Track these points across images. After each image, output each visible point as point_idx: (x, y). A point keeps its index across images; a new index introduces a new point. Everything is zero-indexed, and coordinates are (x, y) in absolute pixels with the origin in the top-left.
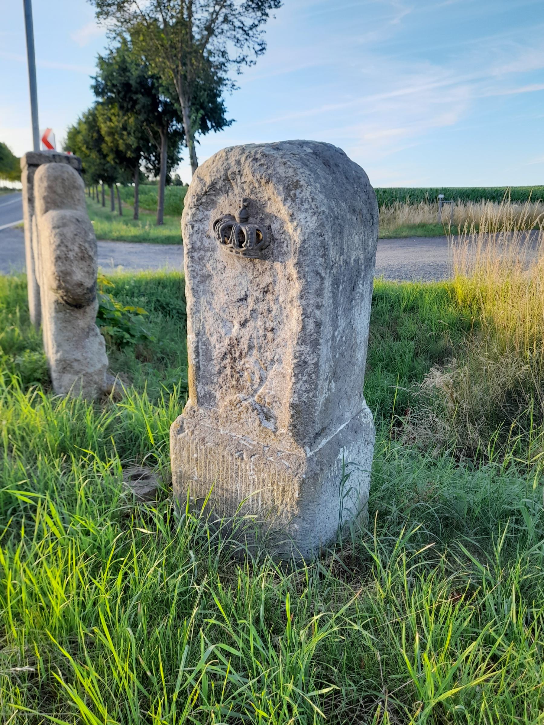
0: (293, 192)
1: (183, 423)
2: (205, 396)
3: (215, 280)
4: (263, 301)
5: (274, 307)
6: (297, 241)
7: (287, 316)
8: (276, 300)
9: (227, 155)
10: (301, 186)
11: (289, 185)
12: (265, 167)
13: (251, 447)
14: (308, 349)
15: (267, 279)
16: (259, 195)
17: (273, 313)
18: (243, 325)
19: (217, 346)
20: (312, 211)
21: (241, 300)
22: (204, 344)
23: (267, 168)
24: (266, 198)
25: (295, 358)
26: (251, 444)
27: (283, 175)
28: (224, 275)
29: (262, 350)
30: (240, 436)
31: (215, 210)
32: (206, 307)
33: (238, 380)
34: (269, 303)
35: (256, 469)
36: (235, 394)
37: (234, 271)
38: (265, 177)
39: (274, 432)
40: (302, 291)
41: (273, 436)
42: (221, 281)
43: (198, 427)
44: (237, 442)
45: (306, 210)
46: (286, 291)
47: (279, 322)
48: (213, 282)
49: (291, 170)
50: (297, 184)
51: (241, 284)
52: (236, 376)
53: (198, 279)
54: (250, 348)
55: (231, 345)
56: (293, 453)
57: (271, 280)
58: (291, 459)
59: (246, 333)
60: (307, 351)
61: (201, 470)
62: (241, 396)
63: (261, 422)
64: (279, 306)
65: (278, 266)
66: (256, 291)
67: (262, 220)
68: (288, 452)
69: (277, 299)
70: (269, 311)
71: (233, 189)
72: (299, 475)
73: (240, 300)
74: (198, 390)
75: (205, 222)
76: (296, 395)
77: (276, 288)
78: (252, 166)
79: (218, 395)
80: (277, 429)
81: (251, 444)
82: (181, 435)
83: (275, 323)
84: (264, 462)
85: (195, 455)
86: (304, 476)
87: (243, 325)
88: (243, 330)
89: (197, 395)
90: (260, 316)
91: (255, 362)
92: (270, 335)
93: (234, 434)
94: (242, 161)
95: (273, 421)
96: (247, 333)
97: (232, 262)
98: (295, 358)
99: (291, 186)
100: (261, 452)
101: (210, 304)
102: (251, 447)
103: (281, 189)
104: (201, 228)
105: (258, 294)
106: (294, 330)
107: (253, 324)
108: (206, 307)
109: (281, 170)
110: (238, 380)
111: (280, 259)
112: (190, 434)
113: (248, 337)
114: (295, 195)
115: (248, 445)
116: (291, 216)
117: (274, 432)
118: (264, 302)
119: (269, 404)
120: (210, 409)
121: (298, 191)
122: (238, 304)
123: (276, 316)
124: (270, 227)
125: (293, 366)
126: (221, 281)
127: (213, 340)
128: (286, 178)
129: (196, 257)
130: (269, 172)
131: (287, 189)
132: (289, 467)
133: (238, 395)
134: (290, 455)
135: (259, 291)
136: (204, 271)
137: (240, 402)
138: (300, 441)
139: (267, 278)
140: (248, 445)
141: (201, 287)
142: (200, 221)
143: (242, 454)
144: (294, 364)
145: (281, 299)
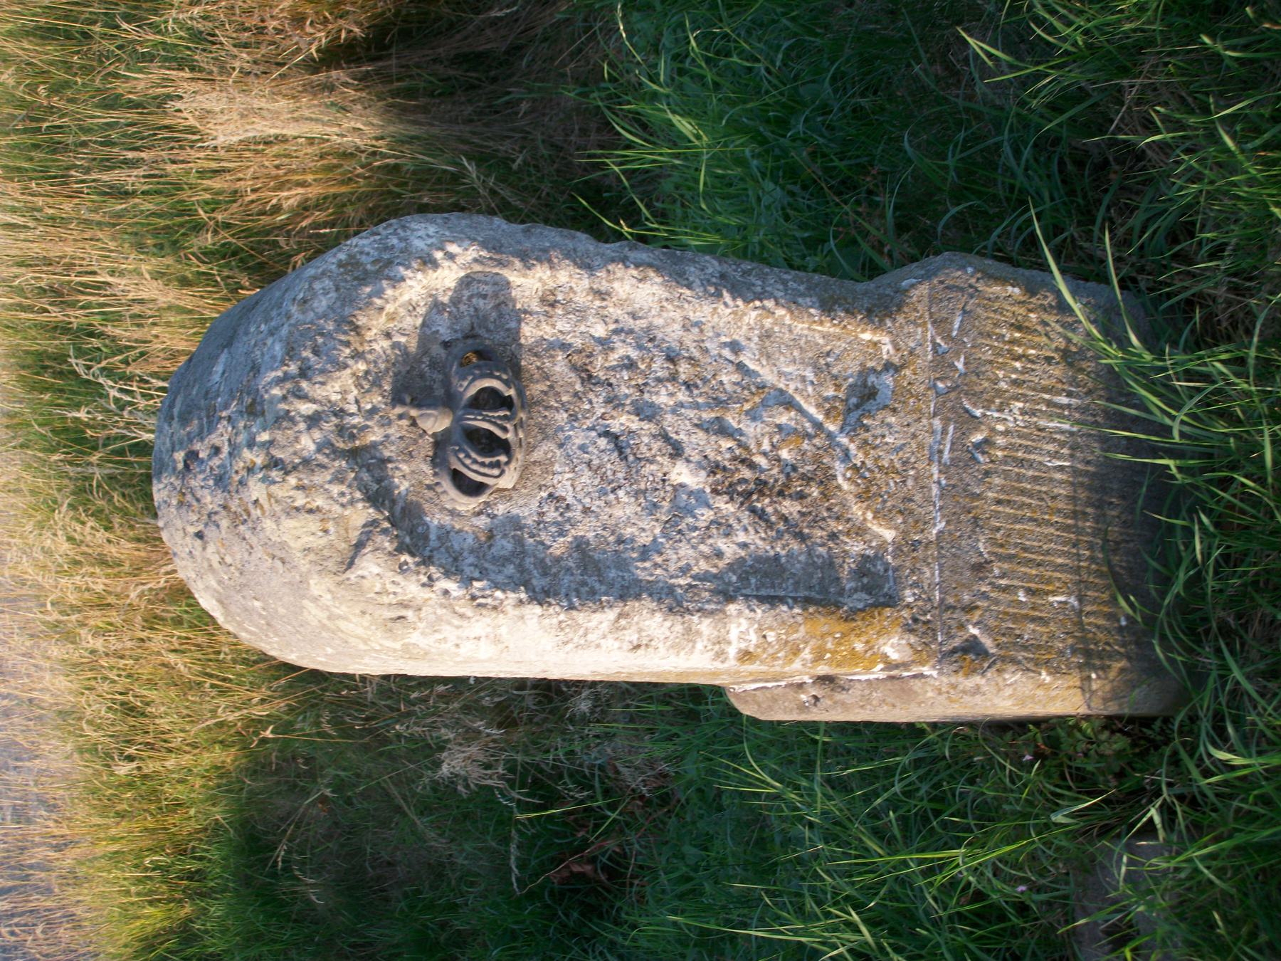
0: (369, 267)
1: (954, 651)
2: (868, 589)
3: (587, 530)
4: (610, 385)
5: (623, 349)
6: (475, 255)
7: (634, 316)
8: (606, 344)
9: (295, 468)
10: (351, 256)
11: (356, 278)
12: (320, 340)
13: (951, 428)
14: (692, 269)
15: (560, 366)
16: (383, 366)
17: (634, 354)
18: (677, 451)
19: (742, 537)
20: (399, 231)
21: (620, 449)
22: (744, 578)
23: (322, 334)
24: (386, 344)
25: (719, 295)
26: (944, 432)
27: (333, 295)
28: (570, 500)
29: (723, 397)
30: (935, 469)
31: (426, 506)
32: (656, 565)
33: (807, 479)
34: (613, 368)
35: (998, 401)
36: (839, 487)
37: (557, 468)
38: (345, 333)
39: (897, 369)
40: (575, 263)
41: (907, 372)
42: (586, 511)
43: (950, 600)
44: (953, 470)
45: (405, 239)
46: (581, 314)
47: (651, 340)
48: (591, 535)
49: (317, 286)
50: (348, 264)
51: (583, 448)
52: (797, 486)
53: (592, 581)
54: (722, 430)
55: (731, 492)
56: (927, 315)
57: (560, 356)
58: (944, 314)
59: (695, 441)
60: (698, 272)
61: (1049, 581)
62: (839, 467)
63: (885, 407)
64: (615, 338)
65: (529, 332)
66: (590, 402)
67: (433, 365)
68: (931, 331)
69: (601, 341)
70: (630, 365)
71: (374, 445)
72: (973, 281)
73: (621, 453)
74: (860, 606)
75: (456, 547)
76: (800, 300)
77: (578, 343)
78: (323, 371)
79: (856, 547)
80: (888, 366)
81: (944, 432)
82: (988, 642)
83: (655, 351)
84: (974, 378)
85: (1022, 596)
86: (970, 270)
87: (677, 451)
88: (688, 451)
89: (872, 605)
90: (646, 396)
91: (754, 419)
92: (684, 369)
93: (935, 490)
94: (306, 408)
95: (872, 379)
96: (693, 439)
97: (538, 470)
98: (719, 295)
99: (356, 274)
100: (953, 395)
101: (645, 553)
102: (951, 428)
103: (368, 290)
104: (471, 560)
105: (598, 399)
106: (661, 292)
107: (669, 417)
108: (656, 565)
109: (322, 304)
110: (807, 479)
111: (513, 325)
112: (976, 616)
113: (701, 434)
114: (374, 262)
115: (949, 437)
116: (425, 263)
117: (897, 369)
118: (613, 381)
119: (838, 387)
120: (896, 570)
121: (364, 259)
122: (631, 458)
123: (640, 347)
124: (446, 345)
125: (740, 302)
126: (586, 511)
127: (730, 550)
128: (337, 289)
129: (545, 582)
130: (330, 326)
131: (364, 279)
132: (965, 312)
133: (840, 480)
134: (934, 323)
135: (591, 396)
136: (571, 564)
137: (855, 469)
138: (896, 301)
139: (557, 369)
140: (949, 437)
141: (613, 573)
142: (456, 559)
143: (977, 446)
144: (734, 299)
145: (600, 331)
